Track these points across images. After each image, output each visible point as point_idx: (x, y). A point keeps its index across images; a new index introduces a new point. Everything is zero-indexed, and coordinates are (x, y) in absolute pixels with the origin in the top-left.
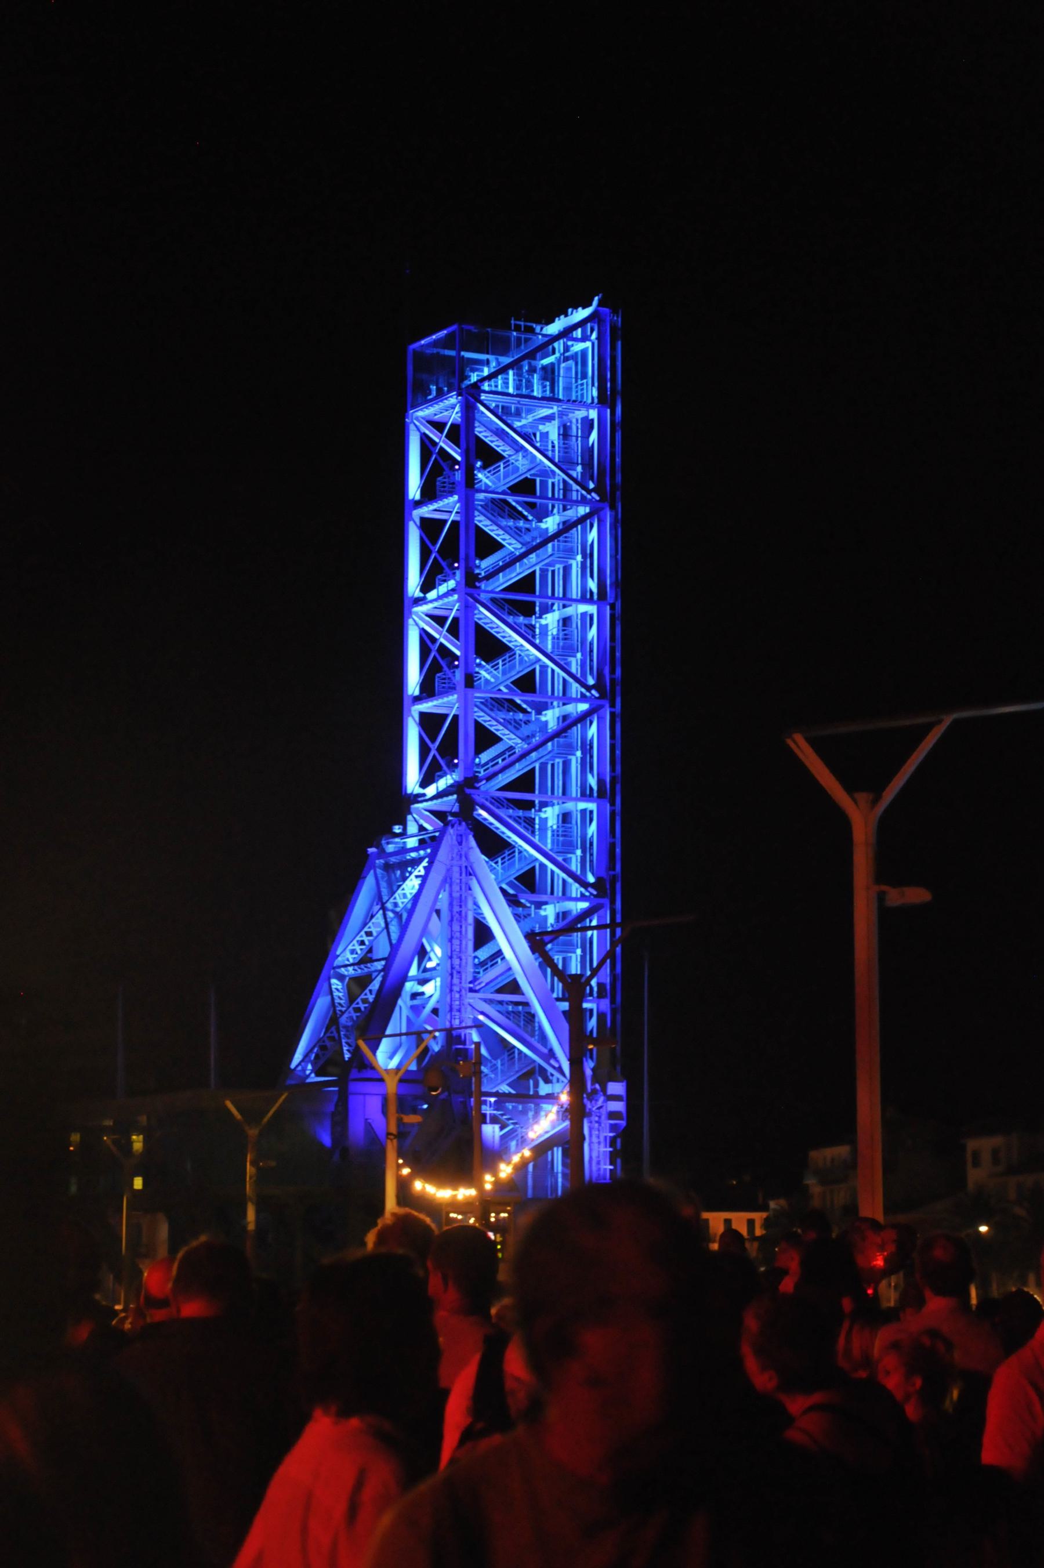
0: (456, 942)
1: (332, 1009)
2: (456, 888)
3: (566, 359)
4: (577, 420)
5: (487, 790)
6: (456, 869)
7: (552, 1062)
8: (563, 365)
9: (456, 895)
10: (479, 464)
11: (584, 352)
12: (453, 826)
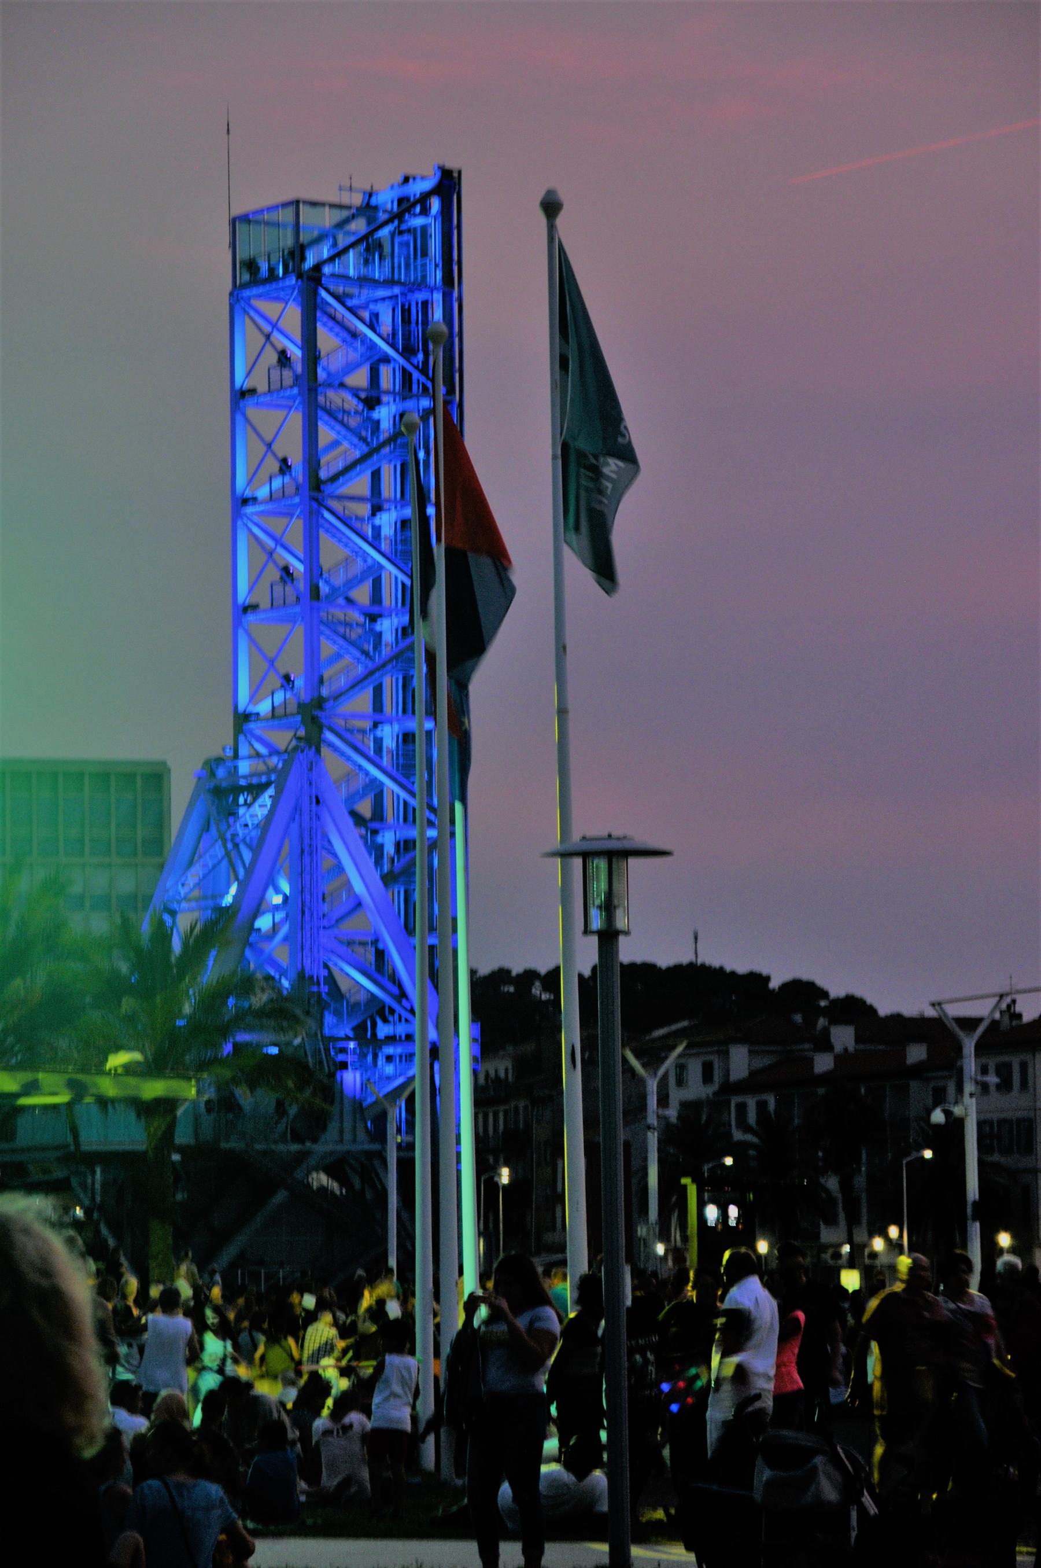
0: (307, 860)
1: (246, 627)
2: (306, 817)
3: (401, 233)
4: (417, 303)
5: (333, 1325)
6: (306, 799)
7: (404, 1001)
8: (397, 240)
9: (306, 825)
10: (823, 1003)
11: (424, 229)
12: (302, 751)
